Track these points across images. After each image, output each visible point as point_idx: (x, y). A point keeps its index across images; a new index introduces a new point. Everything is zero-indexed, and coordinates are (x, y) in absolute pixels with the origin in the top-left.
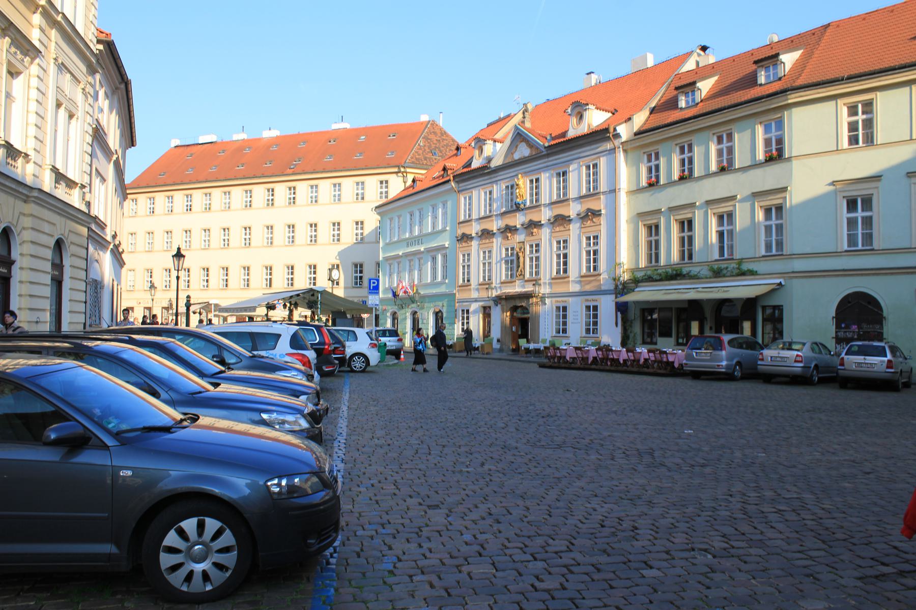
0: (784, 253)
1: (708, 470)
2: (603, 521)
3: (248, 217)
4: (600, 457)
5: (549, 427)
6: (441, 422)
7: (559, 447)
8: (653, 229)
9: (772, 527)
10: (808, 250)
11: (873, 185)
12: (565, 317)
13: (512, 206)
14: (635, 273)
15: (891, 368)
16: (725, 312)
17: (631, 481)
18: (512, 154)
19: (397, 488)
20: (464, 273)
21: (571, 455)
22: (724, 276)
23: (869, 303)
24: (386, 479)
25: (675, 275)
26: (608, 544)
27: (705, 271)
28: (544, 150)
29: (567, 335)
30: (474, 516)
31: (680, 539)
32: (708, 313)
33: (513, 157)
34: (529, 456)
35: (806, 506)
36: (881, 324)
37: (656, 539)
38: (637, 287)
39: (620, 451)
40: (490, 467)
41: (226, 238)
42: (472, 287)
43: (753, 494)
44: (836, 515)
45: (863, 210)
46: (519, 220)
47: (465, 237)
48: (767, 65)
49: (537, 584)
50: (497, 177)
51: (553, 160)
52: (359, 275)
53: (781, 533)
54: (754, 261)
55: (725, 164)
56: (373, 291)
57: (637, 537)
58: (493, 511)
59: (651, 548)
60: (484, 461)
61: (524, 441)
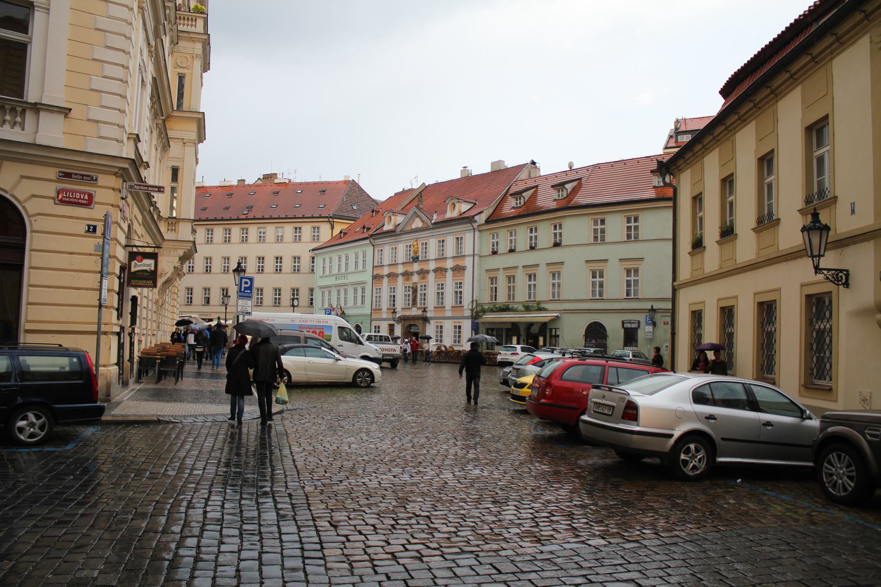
8: (493, 280)
11: (604, 264)
12: (441, 332)
13: (410, 259)
18: (411, 224)
20: (376, 301)
22: (530, 310)
23: (601, 328)
25: (505, 309)
27: (521, 308)
29: (461, 344)
36: (606, 339)
38: (484, 315)
41: (261, 265)
42: (466, 307)
46: (416, 267)
51: (436, 232)
52: (190, 296)
55: (533, 245)
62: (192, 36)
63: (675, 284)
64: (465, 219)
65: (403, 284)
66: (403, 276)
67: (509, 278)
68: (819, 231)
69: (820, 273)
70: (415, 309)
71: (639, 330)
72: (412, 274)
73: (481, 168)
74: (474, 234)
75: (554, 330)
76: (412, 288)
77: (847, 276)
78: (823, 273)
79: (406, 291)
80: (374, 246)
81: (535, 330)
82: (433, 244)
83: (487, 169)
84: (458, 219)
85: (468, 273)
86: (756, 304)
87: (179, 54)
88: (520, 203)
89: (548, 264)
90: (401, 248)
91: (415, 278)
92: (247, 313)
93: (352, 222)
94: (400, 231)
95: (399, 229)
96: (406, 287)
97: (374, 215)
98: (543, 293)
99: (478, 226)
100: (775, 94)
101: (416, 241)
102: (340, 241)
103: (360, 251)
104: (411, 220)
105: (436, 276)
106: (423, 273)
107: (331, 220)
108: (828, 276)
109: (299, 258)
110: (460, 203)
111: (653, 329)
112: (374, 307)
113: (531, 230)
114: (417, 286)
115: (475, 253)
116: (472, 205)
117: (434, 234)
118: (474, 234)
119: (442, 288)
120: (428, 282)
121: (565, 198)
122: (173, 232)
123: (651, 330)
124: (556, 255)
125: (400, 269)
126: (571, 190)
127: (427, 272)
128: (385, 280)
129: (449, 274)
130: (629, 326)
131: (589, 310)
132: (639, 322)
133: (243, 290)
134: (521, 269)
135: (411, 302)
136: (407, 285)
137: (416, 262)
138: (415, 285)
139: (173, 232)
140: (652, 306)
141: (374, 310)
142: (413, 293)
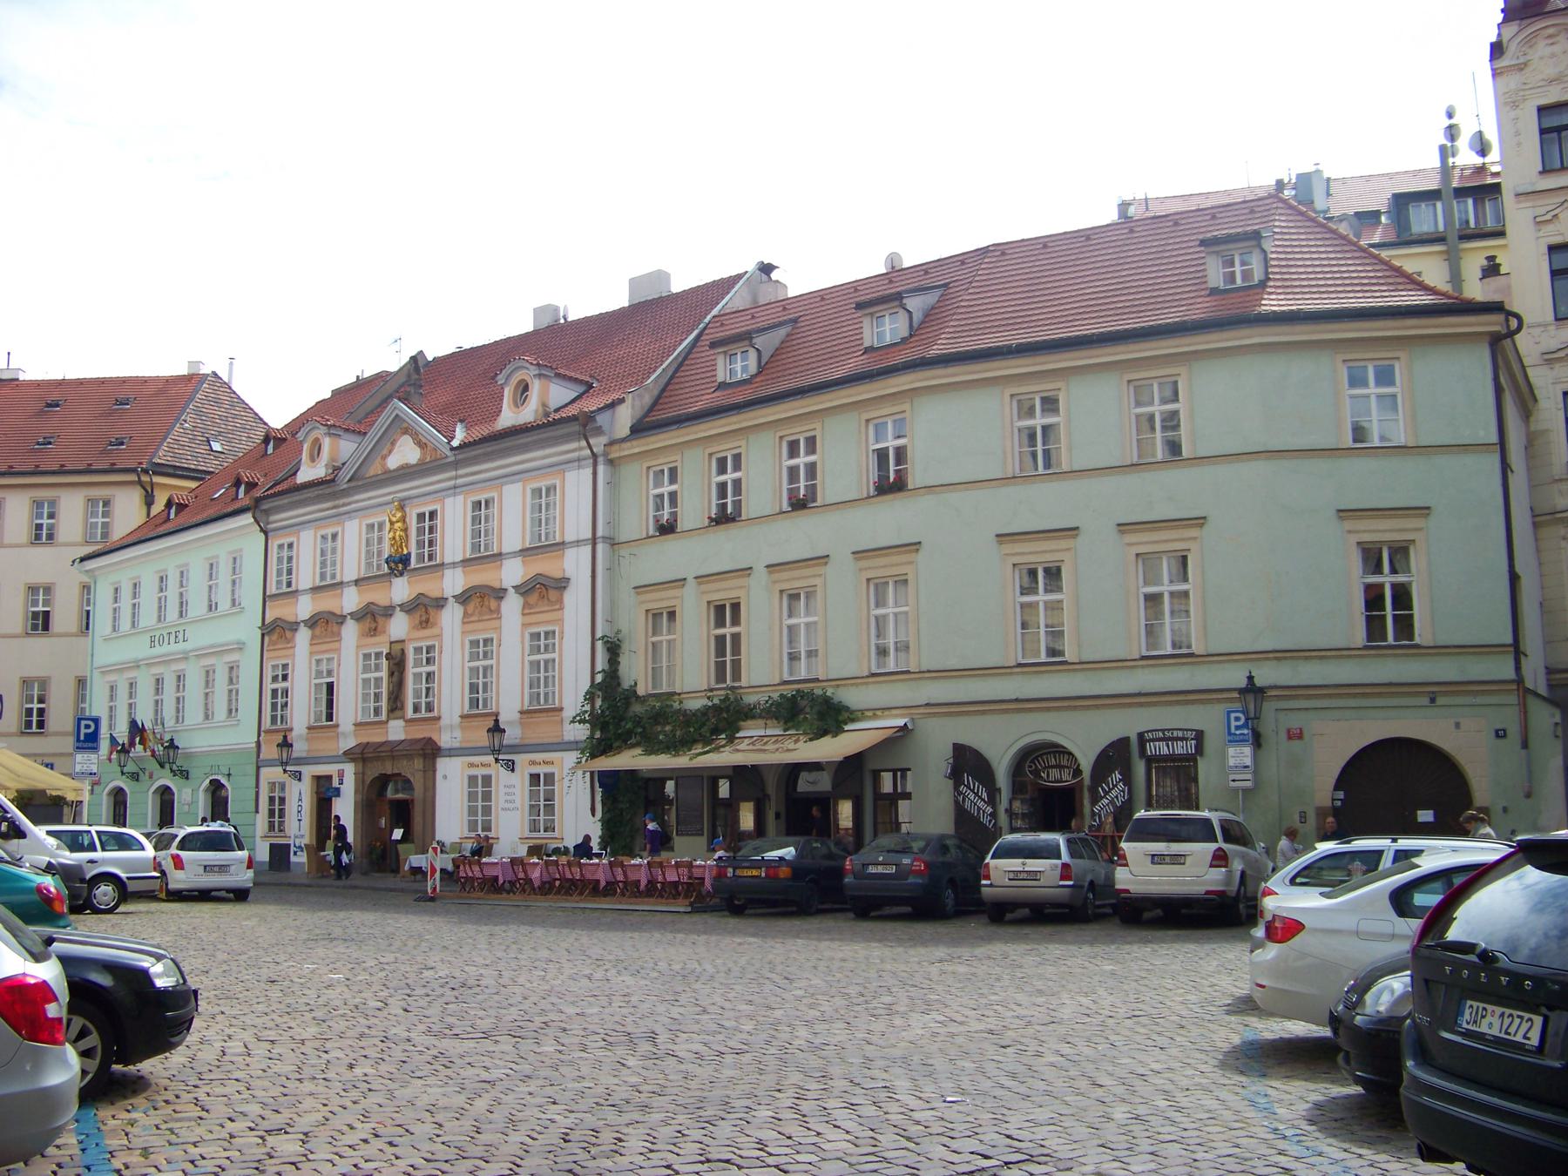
0: (743, 685)
1: (747, 1058)
2: (567, 1134)
4: (561, 1048)
5: (465, 1005)
6: (258, 1003)
7: (486, 1035)
9: (835, 1126)
10: (953, 663)
11: (1063, 544)
12: (487, 796)
15: (1069, 878)
16: (804, 784)
17: (616, 1081)
18: (384, 458)
19: (203, 1110)
21: (508, 1048)
24: (177, 1097)
26: (575, 1162)
28: (449, 453)
30: (352, 1138)
31: (690, 1149)
32: (771, 789)
33: (384, 465)
34: (434, 1052)
35: (894, 1096)
37: (651, 1151)
39: (596, 1037)
40: (366, 1071)
43: (814, 1086)
44: (934, 1105)
45: (1046, 591)
46: (401, 590)
47: (278, 630)
48: (881, 314)
50: (349, 504)
53: (848, 1132)
54: (857, 685)
56: (86, 745)
57: (622, 1151)
58: (381, 1131)
59: (643, 1164)
60: (354, 1062)
61: (422, 1027)
66: (358, 620)
70: (401, 723)
71: (1203, 765)
72: (388, 611)
74: (595, 474)
77: (513, 764)
79: (366, 669)
80: (266, 533)
82: (455, 518)
83: (619, 299)
84: (544, 426)
85: (576, 601)
88: (745, 369)
89: (859, 554)
91: (399, 626)
94: (349, 481)
95: (345, 475)
96: (367, 656)
97: (270, 450)
99: (612, 443)
101: (402, 508)
103: (222, 553)
104: (387, 441)
105: (466, 614)
106: (424, 609)
107: (145, 478)
109: (48, 590)
111: (1255, 757)
112: (267, 723)
114: (403, 650)
115: (600, 533)
116: (582, 389)
117: (460, 481)
118: (595, 474)
119: (485, 654)
123: (1248, 761)
125: (351, 600)
127: (440, 603)
128: (303, 636)
129: (512, 606)
130: (1165, 751)
131: (1017, 700)
132: (1199, 736)
134: (760, 577)
135: (384, 703)
136: (373, 650)
137: (402, 574)
138: (397, 647)
140: (1250, 678)
141: (267, 732)
142: (391, 674)
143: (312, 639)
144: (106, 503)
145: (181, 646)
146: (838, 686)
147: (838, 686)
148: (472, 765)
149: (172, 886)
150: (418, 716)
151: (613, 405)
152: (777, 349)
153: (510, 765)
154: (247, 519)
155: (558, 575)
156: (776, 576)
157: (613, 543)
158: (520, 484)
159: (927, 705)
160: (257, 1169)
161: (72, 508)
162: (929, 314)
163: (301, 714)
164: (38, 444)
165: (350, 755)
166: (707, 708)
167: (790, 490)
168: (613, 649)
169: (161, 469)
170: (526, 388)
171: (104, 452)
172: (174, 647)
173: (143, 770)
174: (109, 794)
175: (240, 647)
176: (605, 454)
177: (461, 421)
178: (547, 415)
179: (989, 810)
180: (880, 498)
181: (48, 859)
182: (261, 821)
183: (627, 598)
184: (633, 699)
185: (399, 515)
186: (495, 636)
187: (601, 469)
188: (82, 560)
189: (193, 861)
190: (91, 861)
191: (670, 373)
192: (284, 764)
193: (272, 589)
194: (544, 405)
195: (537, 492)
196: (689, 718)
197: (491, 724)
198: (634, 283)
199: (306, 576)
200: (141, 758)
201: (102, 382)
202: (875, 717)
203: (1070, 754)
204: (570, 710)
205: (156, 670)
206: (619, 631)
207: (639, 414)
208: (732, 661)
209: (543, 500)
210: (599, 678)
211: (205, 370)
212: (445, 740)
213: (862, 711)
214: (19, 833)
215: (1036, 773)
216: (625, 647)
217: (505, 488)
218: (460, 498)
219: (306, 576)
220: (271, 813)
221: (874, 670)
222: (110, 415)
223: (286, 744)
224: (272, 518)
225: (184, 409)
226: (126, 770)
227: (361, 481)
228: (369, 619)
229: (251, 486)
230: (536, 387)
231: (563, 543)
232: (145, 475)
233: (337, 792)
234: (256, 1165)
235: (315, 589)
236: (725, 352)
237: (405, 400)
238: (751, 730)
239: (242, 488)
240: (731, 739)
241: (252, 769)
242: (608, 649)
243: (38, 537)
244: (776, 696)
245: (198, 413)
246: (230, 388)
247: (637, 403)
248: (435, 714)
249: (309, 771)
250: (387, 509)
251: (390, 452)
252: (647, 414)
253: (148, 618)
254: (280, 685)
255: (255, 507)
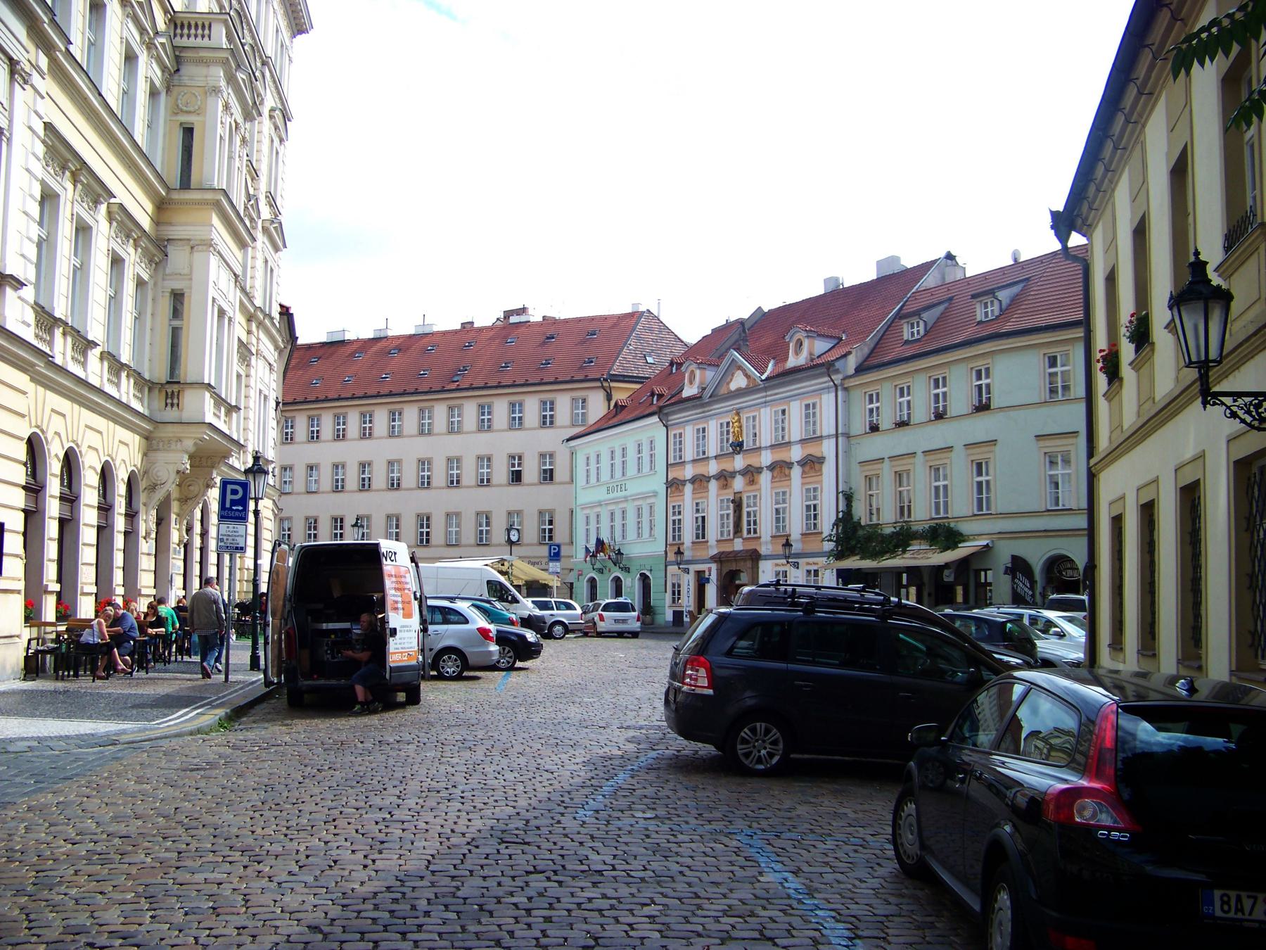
0: (949, 516)
3: (453, 445)
11: (1070, 441)
14: (595, 567)
18: (728, 384)
32: (926, 579)
33: (728, 388)
46: (739, 462)
47: (675, 485)
49: (619, 839)
50: (711, 410)
62: (203, 54)
63: (1093, 461)
64: (820, 368)
65: (718, 495)
66: (717, 479)
67: (899, 475)
68: (1200, 305)
69: (1214, 404)
70: (740, 540)
72: (733, 475)
73: (859, 272)
75: (983, 573)
76: (733, 501)
78: (1223, 403)
80: (667, 427)
81: (948, 577)
82: (766, 418)
83: (869, 275)
85: (828, 469)
86: (1178, 490)
87: (181, 88)
88: (918, 333)
90: (713, 428)
91: (739, 483)
92: (237, 548)
93: (638, 386)
94: (710, 397)
98: (961, 505)
100: (1181, 20)
101: (738, 414)
102: (611, 422)
103: (644, 437)
106: (751, 473)
107: (606, 384)
108: (1235, 409)
110: (811, 339)
113: (937, 381)
114: (741, 498)
115: (840, 431)
116: (836, 341)
117: (768, 399)
120: (760, 489)
121: (997, 317)
122: (175, 408)
124: (982, 427)
126: (1008, 302)
127: (759, 470)
128: (688, 488)
129: (796, 472)
131: (1045, 531)
133: (228, 505)
137: (739, 453)
138: (738, 496)
139: (175, 408)
141: (670, 545)
142: (735, 511)
143: (693, 490)
144: (584, 401)
145: (624, 493)
146: (957, 521)
147: (957, 521)
148: (777, 565)
149: (599, 630)
150: (749, 536)
151: (845, 356)
152: (938, 318)
153: (796, 566)
154: (655, 419)
155: (819, 455)
156: (927, 458)
157: (847, 436)
158: (799, 401)
159: (999, 533)
160: (735, 853)
161: (563, 404)
162: (1014, 301)
163: (688, 535)
164: (542, 364)
165: (714, 559)
166: (893, 532)
167: (935, 408)
168: (849, 498)
169: (616, 378)
170: (801, 344)
171: (581, 368)
172: (620, 494)
173: (605, 567)
174: (587, 581)
175: (655, 494)
176: (842, 385)
177: (774, 358)
178: (812, 360)
179: (1030, 593)
180: (977, 414)
181: (529, 613)
182: (668, 596)
183: (856, 469)
184: (858, 528)
185: (736, 418)
186: (788, 490)
187: (840, 393)
188: (568, 440)
189: (609, 617)
190: (552, 615)
191: (882, 332)
192: (678, 564)
193: (671, 461)
194: (811, 354)
195: (807, 406)
196: (884, 539)
197: (784, 541)
198: (879, 264)
199: (689, 453)
200: (604, 560)
201: (579, 320)
202: (974, 540)
203: (1073, 561)
204: (826, 532)
205: (612, 507)
206: (851, 489)
207: (860, 360)
208: (944, 501)
209: (810, 411)
210: (841, 515)
211: (642, 308)
212: (763, 550)
213: (968, 536)
214: (515, 601)
215: (1060, 572)
216: (855, 497)
217: (791, 403)
218: (768, 409)
219: (689, 453)
220: (674, 593)
221: (976, 512)
222: (584, 342)
223: (679, 553)
224: (670, 418)
225: (629, 336)
226: (595, 567)
227: (716, 398)
228: (722, 480)
229: (660, 396)
230: (806, 343)
231: (821, 437)
232: (607, 381)
233: (708, 580)
234: (736, 850)
235: (694, 461)
236: (908, 322)
237: (737, 350)
238: (915, 546)
239: (655, 397)
240: (904, 551)
241: (663, 567)
242: (846, 499)
243: (544, 423)
244: (927, 526)
245: (639, 338)
246: (659, 320)
247: (859, 354)
248: (758, 535)
249: (693, 568)
250: (730, 415)
251: (731, 380)
252: (865, 361)
253: (605, 476)
254: (677, 518)
255: (659, 412)
